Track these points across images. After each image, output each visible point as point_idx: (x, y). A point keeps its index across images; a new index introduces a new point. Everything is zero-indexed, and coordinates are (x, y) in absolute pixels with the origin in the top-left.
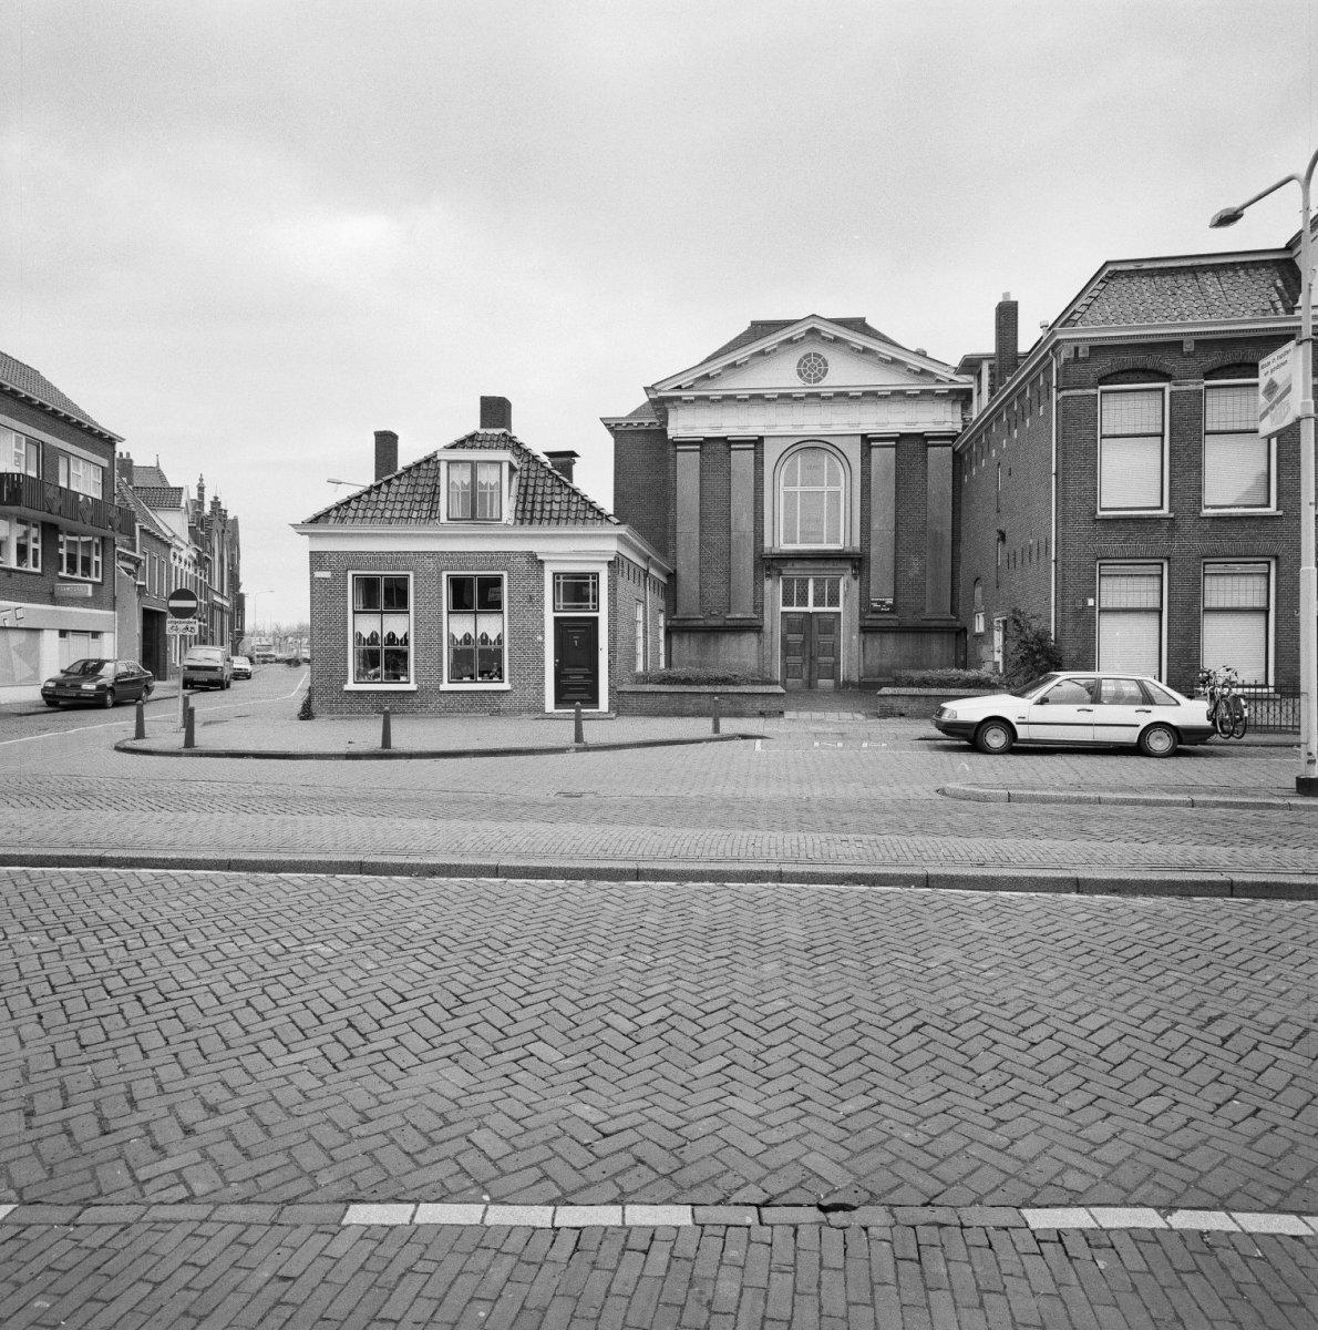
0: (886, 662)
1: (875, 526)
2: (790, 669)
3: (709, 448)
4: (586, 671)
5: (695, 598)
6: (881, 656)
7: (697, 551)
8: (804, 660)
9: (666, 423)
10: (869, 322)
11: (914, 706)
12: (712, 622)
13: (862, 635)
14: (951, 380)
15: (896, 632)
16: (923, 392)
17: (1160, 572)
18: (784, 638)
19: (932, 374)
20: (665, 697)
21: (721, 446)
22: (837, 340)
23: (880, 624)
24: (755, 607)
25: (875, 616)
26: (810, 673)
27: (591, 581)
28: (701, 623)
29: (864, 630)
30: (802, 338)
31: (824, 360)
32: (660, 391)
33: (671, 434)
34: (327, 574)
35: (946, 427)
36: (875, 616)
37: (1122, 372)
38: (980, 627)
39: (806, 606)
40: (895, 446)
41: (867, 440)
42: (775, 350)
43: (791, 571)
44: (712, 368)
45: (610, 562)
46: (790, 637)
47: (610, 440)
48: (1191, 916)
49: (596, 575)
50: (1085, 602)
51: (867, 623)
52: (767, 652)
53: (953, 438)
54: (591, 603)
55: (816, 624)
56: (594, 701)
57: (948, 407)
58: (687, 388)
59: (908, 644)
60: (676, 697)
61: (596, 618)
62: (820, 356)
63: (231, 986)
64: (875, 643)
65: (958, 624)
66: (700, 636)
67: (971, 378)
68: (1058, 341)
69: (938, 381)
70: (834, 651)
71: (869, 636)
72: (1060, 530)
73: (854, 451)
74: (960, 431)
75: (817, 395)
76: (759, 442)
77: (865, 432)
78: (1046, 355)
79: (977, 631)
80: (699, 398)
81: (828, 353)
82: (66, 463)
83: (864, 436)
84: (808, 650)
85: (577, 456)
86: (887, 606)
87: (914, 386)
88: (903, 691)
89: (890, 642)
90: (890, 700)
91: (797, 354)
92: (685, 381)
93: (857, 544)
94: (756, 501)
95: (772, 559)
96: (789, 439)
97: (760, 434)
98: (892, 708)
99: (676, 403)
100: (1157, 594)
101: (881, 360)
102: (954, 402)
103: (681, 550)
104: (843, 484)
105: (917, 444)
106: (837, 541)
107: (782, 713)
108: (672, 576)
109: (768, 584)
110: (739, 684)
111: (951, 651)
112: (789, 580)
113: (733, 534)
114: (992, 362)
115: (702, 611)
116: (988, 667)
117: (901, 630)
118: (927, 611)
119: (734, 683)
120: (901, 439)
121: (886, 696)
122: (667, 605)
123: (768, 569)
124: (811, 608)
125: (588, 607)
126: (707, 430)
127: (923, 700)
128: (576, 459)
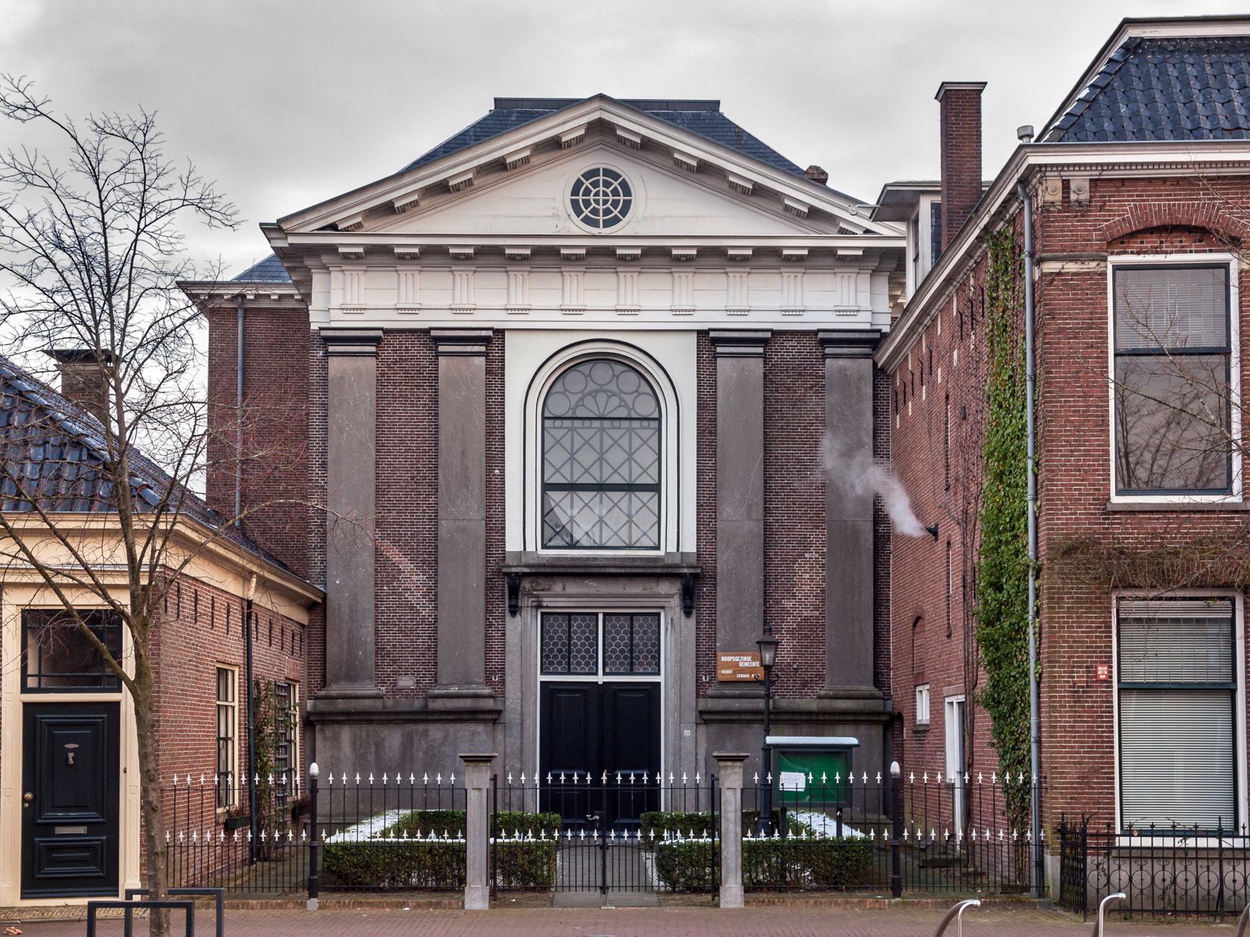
5: (371, 647)
9: (306, 298)
10: (728, 111)
14: (867, 231)
16: (814, 252)
17: (1229, 616)
19: (830, 218)
22: (648, 145)
28: (378, 705)
30: (579, 140)
31: (624, 185)
33: (317, 320)
34: (71, 761)
35: (861, 322)
37: (1150, 231)
38: (923, 714)
40: (764, 356)
44: (400, 194)
50: (1092, 670)
51: (712, 704)
57: (864, 280)
58: (347, 231)
62: (616, 176)
67: (901, 227)
68: (1031, 167)
69: (842, 231)
74: (886, 329)
75: (609, 252)
77: (705, 327)
78: (1013, 193)
80: (372, 250)
81: (629, 170)
82: (212, 912)
83: (702, 334)
87: (797, 239)
91: (574, 168)
92: (344, 216)
93: (690, 546)
97: (497, 326)
99: (325, 259)
100: (1225, 649)
102: (875, 273)
108: (317, 607)
114: (938, 199)
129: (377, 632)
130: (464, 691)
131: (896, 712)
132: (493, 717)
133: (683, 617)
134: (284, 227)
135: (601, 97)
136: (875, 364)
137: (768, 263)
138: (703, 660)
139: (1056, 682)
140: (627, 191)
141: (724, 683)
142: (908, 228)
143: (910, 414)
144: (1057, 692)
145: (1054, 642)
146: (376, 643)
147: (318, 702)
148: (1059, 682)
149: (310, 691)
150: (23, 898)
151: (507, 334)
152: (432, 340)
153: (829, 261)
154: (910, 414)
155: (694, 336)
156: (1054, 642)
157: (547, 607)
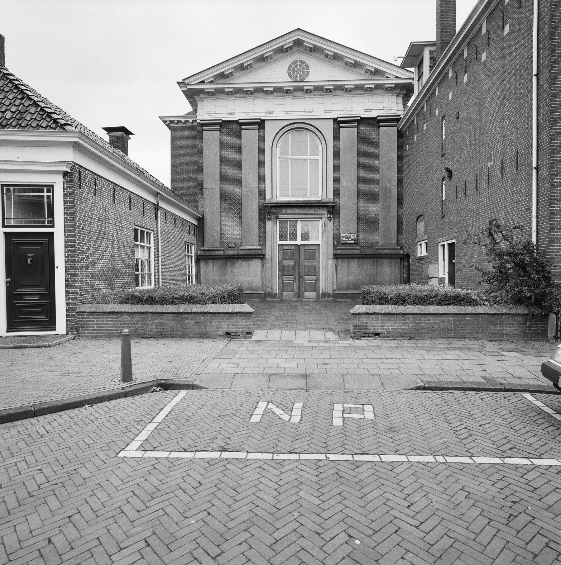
0: (352, 279)
1: (344, 183)
2: (285, 286)
3: (226, 128)
4: (42, 290)
5: (217, 235)
6: (349, 275)
7: (218, 201)
8: (295, 278)
11: (389, 325)
12: (230, 252)
13: (335, 261)
14: (397, 77)
15: (359, 258)
18: (280, 263)
20: (126, 318)
21: (235, 127)
23: (348, 252)
24: (260, 241)
25: (344, 247)
26: (299, 288)
27: (45, 194)
28: (222, 253)
29: (336, 257)
30: (291, 48)
32: (188, 84)
35: (393, 113)
36: (344, 247)
38: (422, 251)
39: (296, 240)
41: (337, 122)
42: (271, 56)
43: (284, 214)
45: (65, 174)
46: (285, 262)
47: (168, 132)
48: (530, 428)
49: (50, 188)
51: (338, 251)
52: (269, 273)
53: (398, 121)
54: (46, 218)
55: (302, 253)
56: (51, 323)
57: (394, 97)
59: (367, 266)
60: (138, 317)
61: (52, 234)
62: (303, 63)
63: (11, 453)
64: (344, 265)
65: (402, 252)
66: (220, 262)
69: (387, 77)
70: (315, 271)
71: (340, 260)
72: (543, 135)
73: (328, 129)
76: (261, 124)
77: (336, 117)
79: (419, 255)
81: (309, 60)
83: (335, 120)
84: (297, 271)
85: (132, 134)
86: (352, 240)
87: (371, 82)
88: (377, 308)
89: (354, 264)
90: (364, 319)
93: (331, 196)
94: (259, 166)
95: (272, 207)
96: (282, 121)
98: (366, 327)
99: (202, 96)
101: (347, 63)
102: (398, 95)
103: (207, 201)
104: (320, 155)
105: (372, 125)
106: (317, 195)
107: (249, 333)
108: (201, 220)
109: (269, 224)
110: (204, 303)
111: (397, 271)
112: (284, 222)
113: (244, 189)
115: (222, 244)
116: (434, 283)
117: (362, 256)
118: (380, 243)
119: (198, 302)
120: (361, 121)
121: (360, 314)
122: (198, 240)
123: (269, 214)
124: (299, 242)
125: (43, 222)
126: (225, 115)
127: (398, 318)
128: (130, 136)
129: (221, 228)
130: (251, 248)
131: (405, 254)
132: (262, 257)
133: (328, 222)
134: (186, 82)
135: (298, 29)
136: (398, 129)
137: (360, 93)
138: (335, 236)
139: (554, 215)
140: (308, 68)
141: (343, 244)
142: (415, 69)
143: (407, 149)
144: (555, 221)
145: (554, 193)
146: (221, 232)
147: (201, 252)
148: (556, 215)
149: (199, 248)
150: (7, 332)
151: (266, 122)
152: (238, 124)
153: (360, 92)
154: (407, 149)
155: (332, 120)
156: (554, 193)
157: (280, 218)
